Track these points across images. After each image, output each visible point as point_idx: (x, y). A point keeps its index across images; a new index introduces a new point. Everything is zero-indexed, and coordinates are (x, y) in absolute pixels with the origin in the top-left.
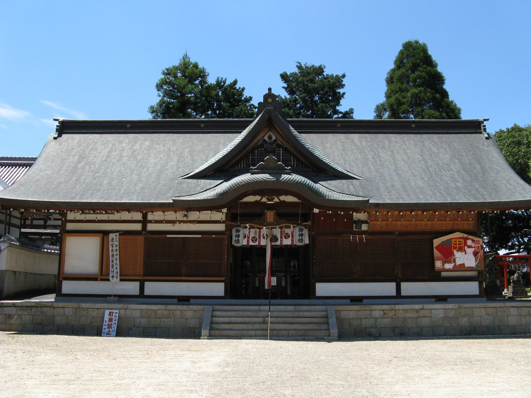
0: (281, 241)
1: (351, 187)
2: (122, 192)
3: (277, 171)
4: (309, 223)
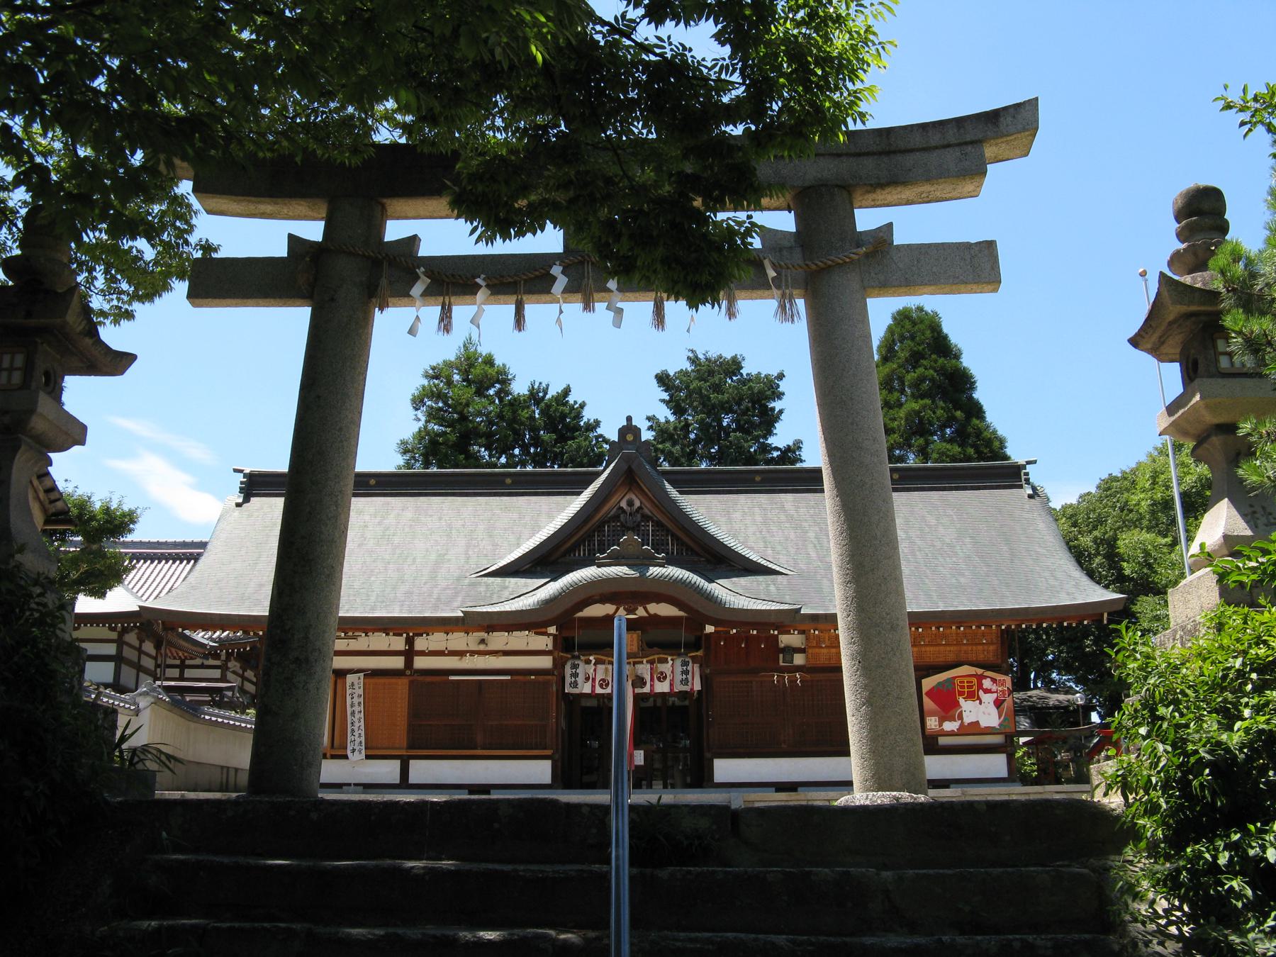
0: (652, 686)
1: (772, 588)
2: (373, 599)
3: (640, 561)
4: (700, 653)
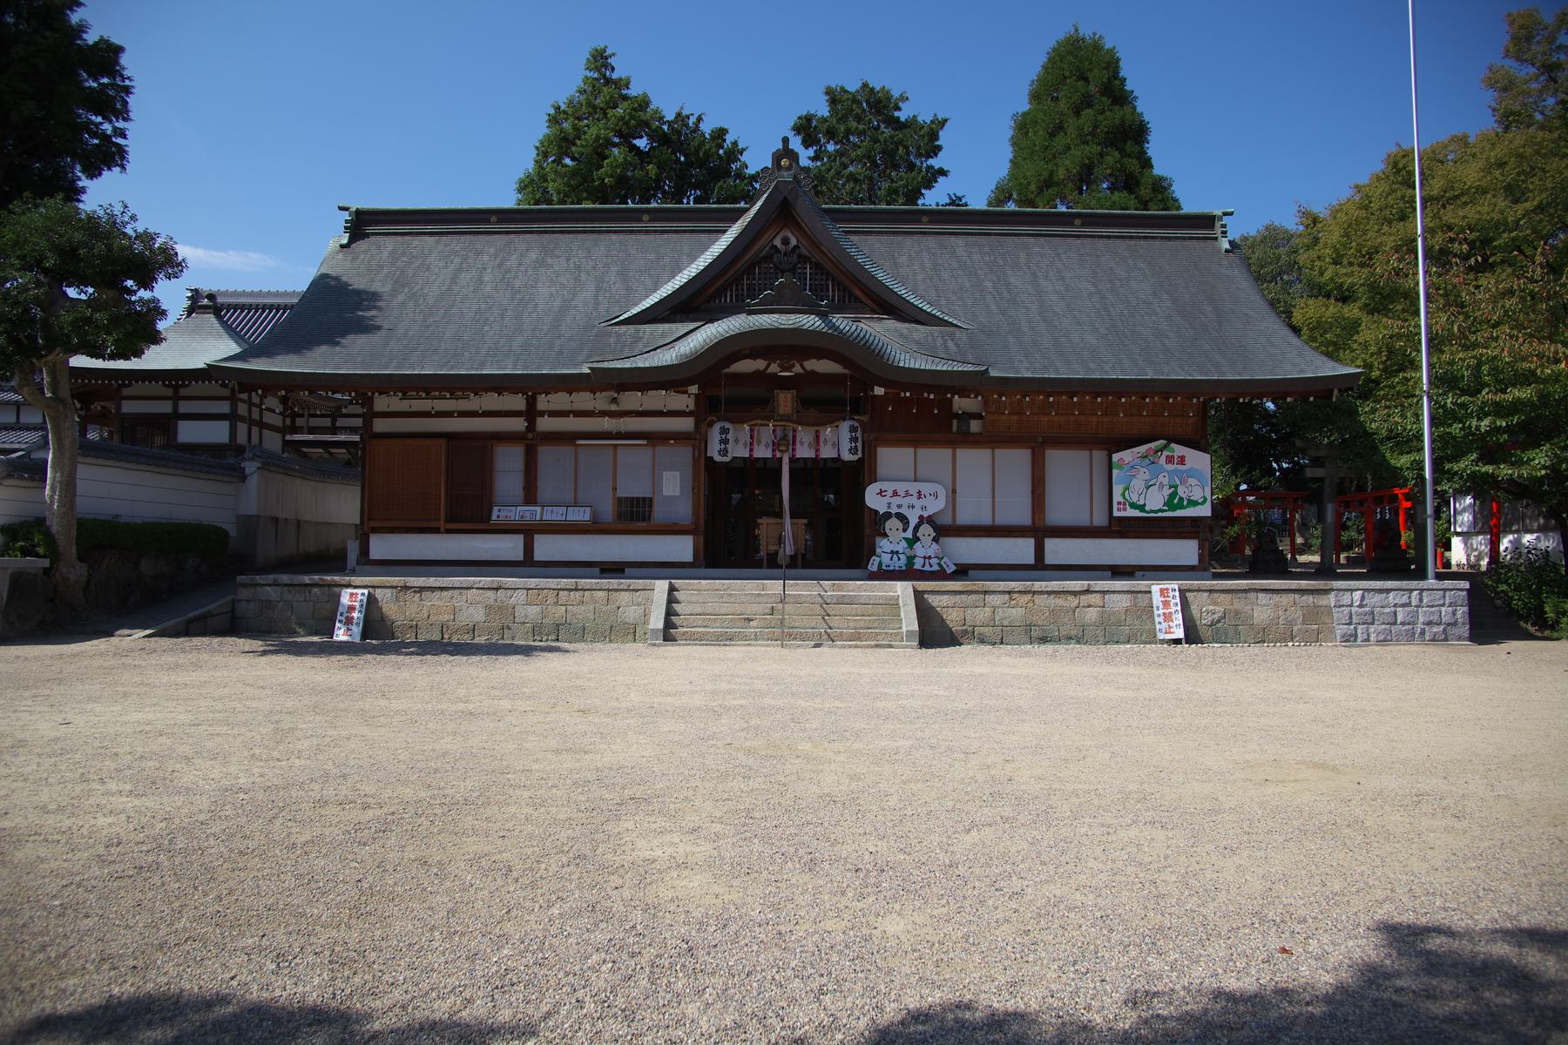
2: (484, 351)
